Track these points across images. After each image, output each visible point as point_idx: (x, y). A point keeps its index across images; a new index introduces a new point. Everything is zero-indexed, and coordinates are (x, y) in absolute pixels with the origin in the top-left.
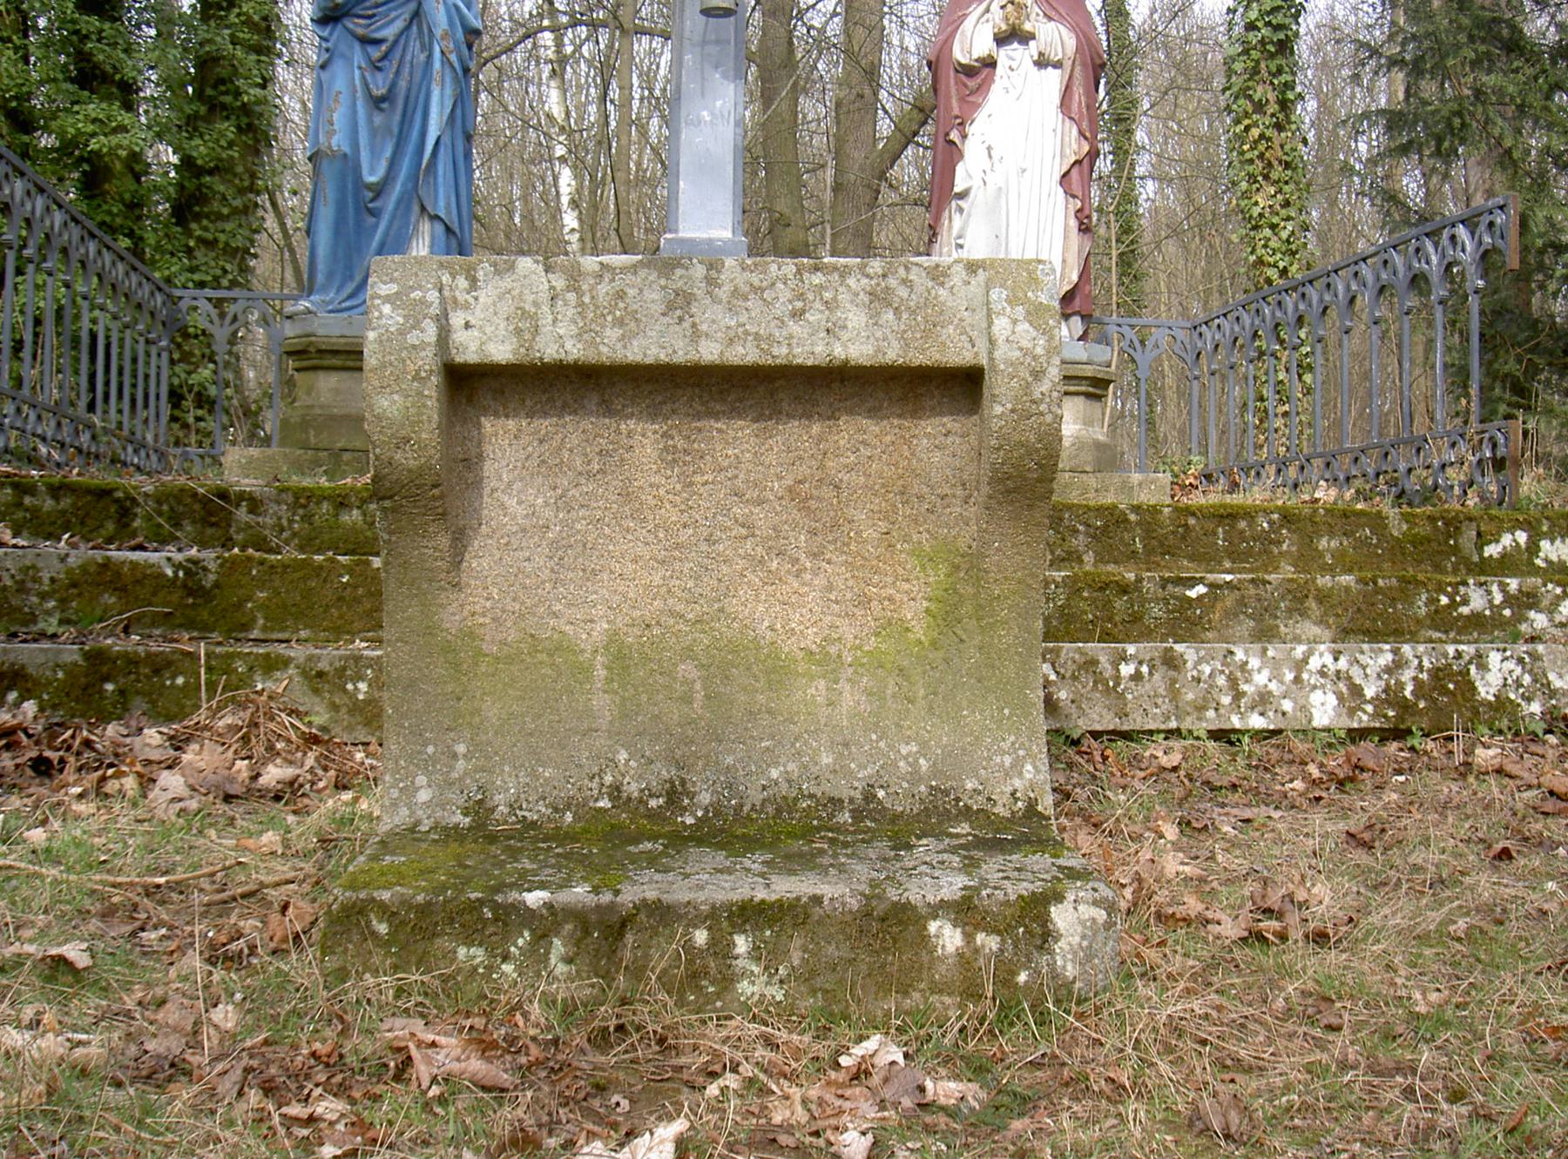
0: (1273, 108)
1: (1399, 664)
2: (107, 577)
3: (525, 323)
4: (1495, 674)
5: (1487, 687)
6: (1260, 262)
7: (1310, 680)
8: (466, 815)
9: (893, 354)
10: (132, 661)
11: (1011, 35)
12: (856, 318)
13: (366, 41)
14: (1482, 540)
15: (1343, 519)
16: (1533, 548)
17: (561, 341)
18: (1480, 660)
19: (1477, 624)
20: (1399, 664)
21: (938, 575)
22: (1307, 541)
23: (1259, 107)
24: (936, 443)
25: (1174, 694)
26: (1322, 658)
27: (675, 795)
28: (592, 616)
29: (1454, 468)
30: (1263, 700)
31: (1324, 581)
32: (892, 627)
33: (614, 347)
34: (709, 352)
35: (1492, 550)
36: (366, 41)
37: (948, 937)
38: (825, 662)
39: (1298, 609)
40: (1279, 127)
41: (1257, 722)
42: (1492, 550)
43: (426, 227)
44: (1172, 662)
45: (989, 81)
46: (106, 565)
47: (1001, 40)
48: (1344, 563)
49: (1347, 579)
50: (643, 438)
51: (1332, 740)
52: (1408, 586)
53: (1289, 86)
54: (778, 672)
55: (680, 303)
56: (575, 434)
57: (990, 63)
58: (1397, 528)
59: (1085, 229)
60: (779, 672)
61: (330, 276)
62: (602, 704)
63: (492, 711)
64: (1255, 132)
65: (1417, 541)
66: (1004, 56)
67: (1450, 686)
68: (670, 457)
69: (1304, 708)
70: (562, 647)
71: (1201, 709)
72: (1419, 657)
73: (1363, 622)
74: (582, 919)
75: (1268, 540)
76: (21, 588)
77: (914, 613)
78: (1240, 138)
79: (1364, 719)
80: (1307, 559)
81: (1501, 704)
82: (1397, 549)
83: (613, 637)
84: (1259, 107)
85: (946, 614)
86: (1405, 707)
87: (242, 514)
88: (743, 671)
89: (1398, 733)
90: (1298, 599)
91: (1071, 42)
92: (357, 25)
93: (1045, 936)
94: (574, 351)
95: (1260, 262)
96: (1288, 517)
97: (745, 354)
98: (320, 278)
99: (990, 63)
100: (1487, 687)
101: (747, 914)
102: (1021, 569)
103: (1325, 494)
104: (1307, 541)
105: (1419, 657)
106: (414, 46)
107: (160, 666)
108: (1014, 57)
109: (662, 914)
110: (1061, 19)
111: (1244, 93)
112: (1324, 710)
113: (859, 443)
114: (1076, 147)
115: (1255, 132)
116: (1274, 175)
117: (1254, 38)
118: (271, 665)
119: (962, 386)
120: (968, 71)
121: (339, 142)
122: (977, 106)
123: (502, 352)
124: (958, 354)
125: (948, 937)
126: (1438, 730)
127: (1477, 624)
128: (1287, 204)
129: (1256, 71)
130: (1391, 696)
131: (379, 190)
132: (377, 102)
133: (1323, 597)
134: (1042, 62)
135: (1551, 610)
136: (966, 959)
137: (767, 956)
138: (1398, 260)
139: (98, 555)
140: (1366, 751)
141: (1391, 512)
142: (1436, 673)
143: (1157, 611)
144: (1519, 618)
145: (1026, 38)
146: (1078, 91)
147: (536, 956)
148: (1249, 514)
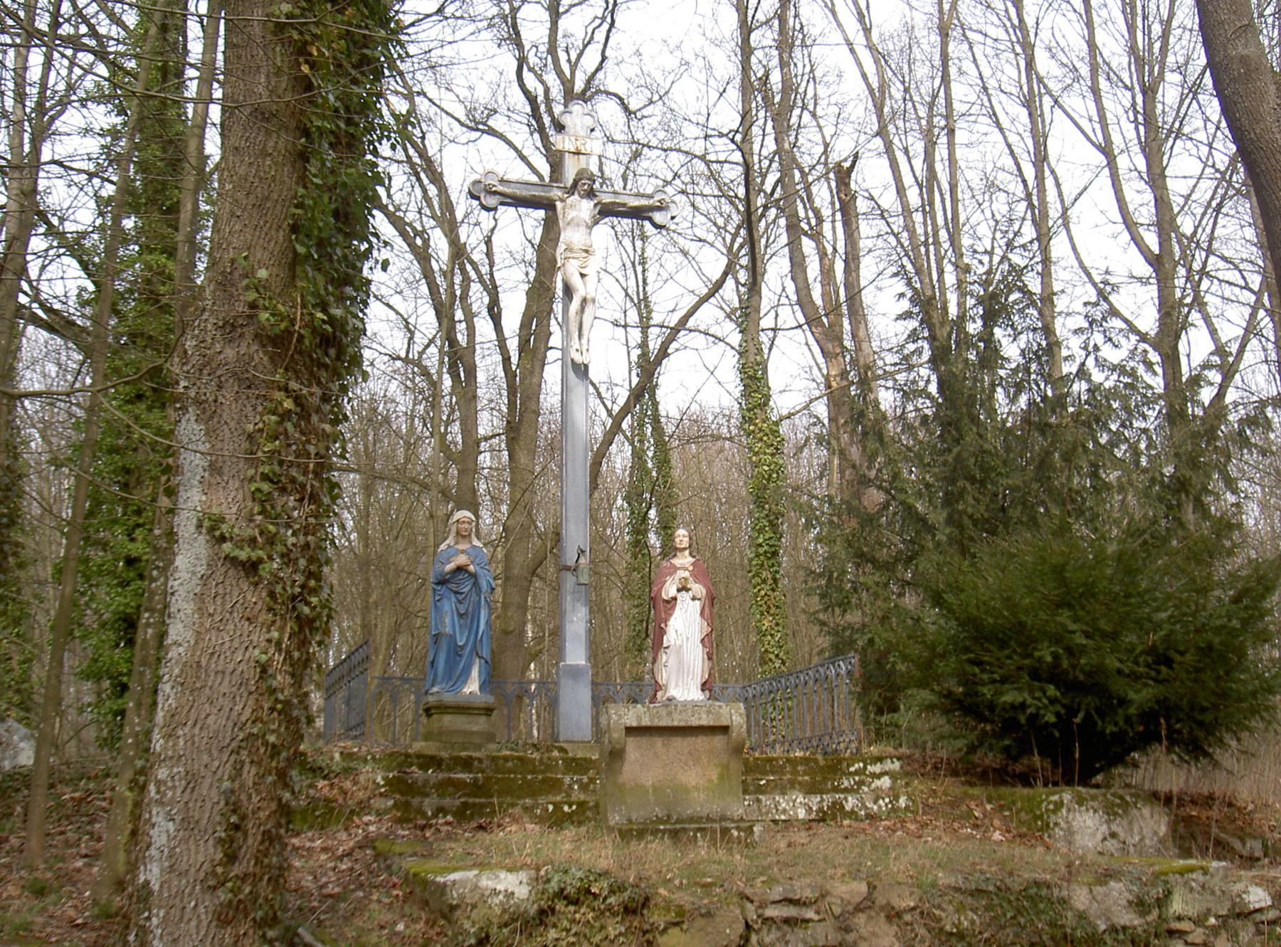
0: (770, 581)
1: (822, 800)
2: (450, 782)
3: (639, 718)
4: (850, 803)
5: (848, 807)
6: (766, 651)
7: (797, 805)
8: (960, 684)
9: (712, 723)
10: (474, 805)
11: (683, 589)
12: (704, 716)
13: (456, 593)
14: (848, 766)
15: (805, 761)
16: (865, 768)
17: (646, 722)
18: (846, 799)
19: (846, 790)
20: (822, 800)
21: (719, 770)
22: (794, 767)
23: (764, 581)
24: (719, 741)
25: (760, 810)
26: (800, 799)
27: (669, 817)
28: (649, 779)
29: (846, 742)
30: (784, 811)
31: (800, 778)
32: (710, 781)
33: (657, 723)
34: (676, 724)
35: (852, 769)
36: (456, 593)
37: (735, 833)
38: (697, 788)
39: (793, 787)
40: (773, 590)
41: (783, 817)
42: (852, 769)
43: (477, 660)
44: (758, 800)
45: (675, 605)
46: (450, 778)
47: (679, 590)
48: (805, 773)
49: (807, 778)
50: (659, 741)
51: (804, 822)
52: (825, 780)
53: (777, 572)
54: (687, 791)
55: (669, 713)
56: (644, 741)
57: (675, 599)
58: (822, 763)
59: (710, 659)
60: (687, 791)
61: (443, 679)
62: (652, 798)
63: (629, 801)
64: (763, 593)
65: (829, 767)
66: (679, 596)
67: (837, 808)
68: (663, 745)
69: (796, 813)
70: (643, 786)
71: (767, 814)
72: (828, 799)
73: (811, 790)
74: (670, 830)
75: (783, 767)
76: (424, 786)
77: (715, 778)
78: (756, 595)
79: (813, 816)
80: (795, 772)
81: (852, 812)
82: (822, 769)
83: (653, 785)
84: (764, 581)
85: (721, 777)
86: (825, 813)
87: (476, 763)
88: (681, 791)
89: (823, 820)
90: (792, 784)
91: (704, 592)
92: (453, 586)
93: (752, 832)
94: (649, 724)
95: (766, 651)
96: (788, 760)
97: (682, 724)
98: (439, 679)
99: (675, 599)
100: (848, 807)
101: (700, 829)
102: (736, 766)
103: (799, 754)
104: (794, 767)
105: (828, 799)
106: (474, 595)
107: (482, 806)
108: (684, 598)
109: (685, 830)
110: (700, 582)
111: (757, 575)
112: (802, 814)
113: (701, 742)
114: (707, 629)
115: (763, 593)
116: (772, 612)
117: (761, 550)
118: (513, 805)
119: (725, 729)
120: (668, 602)
121: (448, 630)
122: (671, 615)
123: (635, 724)
124: (725, 722)
125: (735, 833)
126: (834, 818)
127: (846, 790)
128: (777, 624)
129: (762, 565)
130: (821, 810)
131: (462, 647)
132: (461, 616)
133: (800, 783)
134: (694, 599)
135: (869, 786)
136: (739, 837)
137: (704, 837)
138: (821, 670)
139: (446, 775)
140: (814, 824)
141: (820, 757)
142: (833, 803)
143: (752, 788)
144: (859, 788)
145: (688, 590)
146: (707, 611)
147: (662, 838)
148: (776, 759)
